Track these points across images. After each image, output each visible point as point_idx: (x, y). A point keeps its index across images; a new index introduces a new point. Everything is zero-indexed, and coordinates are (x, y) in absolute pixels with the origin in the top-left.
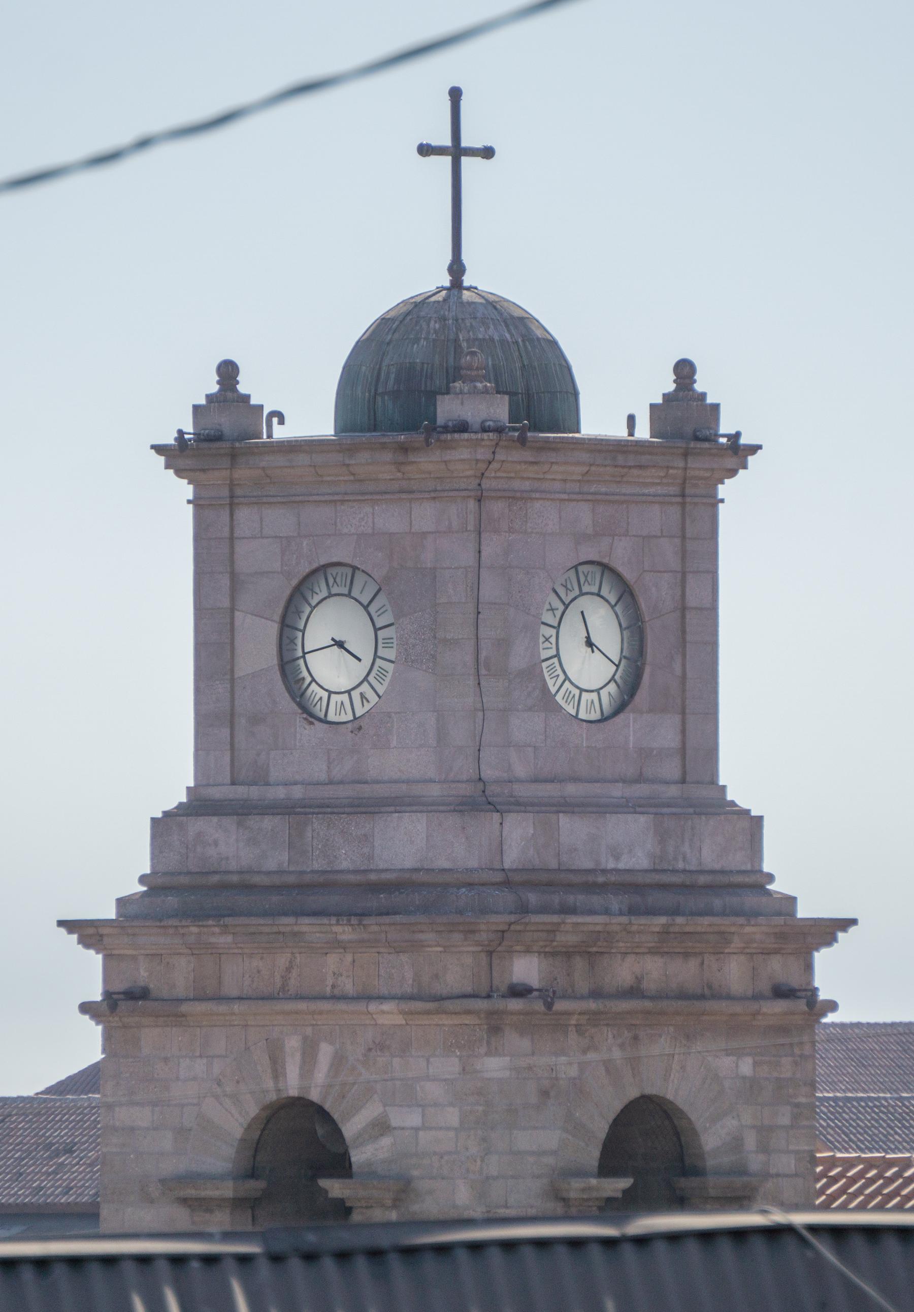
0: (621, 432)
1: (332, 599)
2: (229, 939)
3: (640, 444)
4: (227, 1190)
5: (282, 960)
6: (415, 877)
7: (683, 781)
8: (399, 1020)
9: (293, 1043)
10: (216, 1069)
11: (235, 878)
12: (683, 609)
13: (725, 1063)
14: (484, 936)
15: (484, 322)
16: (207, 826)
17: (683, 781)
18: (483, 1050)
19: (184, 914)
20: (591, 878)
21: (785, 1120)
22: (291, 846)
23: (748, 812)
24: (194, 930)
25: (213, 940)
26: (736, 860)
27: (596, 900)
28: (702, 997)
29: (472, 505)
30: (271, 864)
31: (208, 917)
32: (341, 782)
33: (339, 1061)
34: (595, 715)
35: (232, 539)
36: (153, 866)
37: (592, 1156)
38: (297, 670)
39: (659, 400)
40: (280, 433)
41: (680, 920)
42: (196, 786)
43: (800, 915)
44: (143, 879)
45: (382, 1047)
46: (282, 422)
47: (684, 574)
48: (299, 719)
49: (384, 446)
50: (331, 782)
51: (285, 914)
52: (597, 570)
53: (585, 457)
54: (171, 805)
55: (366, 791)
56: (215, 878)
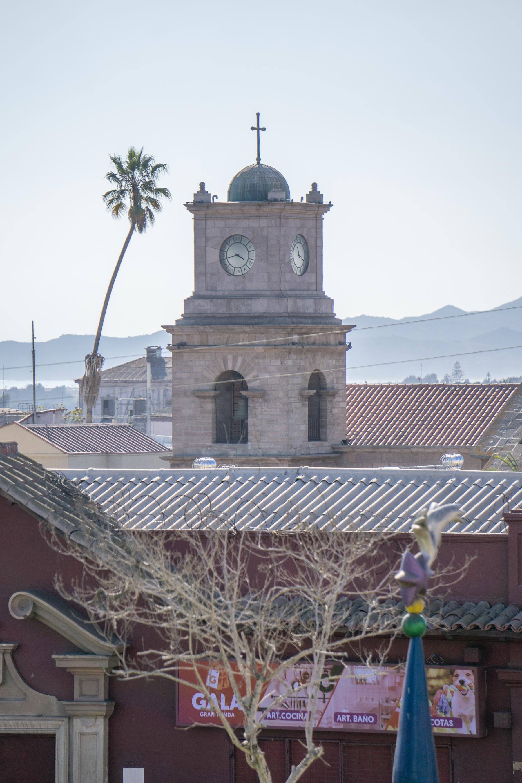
0: (299, 201)
1: (236, 244)
2: (212, 330)
3: (304, 204)
4: (212, 393)
5: (226, 336)
6: (264, 315)
7: (316, 290)
8: (263, 351)
9: (230, 357)
10: (207, 363)
11: (210, 315)
12: (316, 247)
13: (330, 361)
14: (289, 330)
15: (270, 173)
16: (197, 302)
17: (316, 290)
18: (287, 358)
19: (197, 324)
20: (304, 315)
21: (341, 376)
22: (226, 307)
23: (330, 298)
24: (202, 328)
25: (207, 331)
26: (329, 311)
27: (306, 321)
28: (326, 345)
29: (278, 220)
30: (221, 311)
31: (206, 325)
32: (239, 291)
33: (244, 361)
34: (300, 274)
35: (206, 228)
36: (185, 312)
37: (306, 384)
38: (225, 262)
39: (308, 193)
40: (216, 201)
41: (325, 325)
42: (195, 291)
43: (342, 324)
44: (182, 315)
45: (257, 358)
46: (217, 198)
47: (316, 237)
48: (226, 275)
49: (254, 205)
50: (236, 291)
51: (230, 324)
52: (300, 236)
53: (300, 208)
54: (189, 296)
55: (247, 293)
56: (204, 315)
